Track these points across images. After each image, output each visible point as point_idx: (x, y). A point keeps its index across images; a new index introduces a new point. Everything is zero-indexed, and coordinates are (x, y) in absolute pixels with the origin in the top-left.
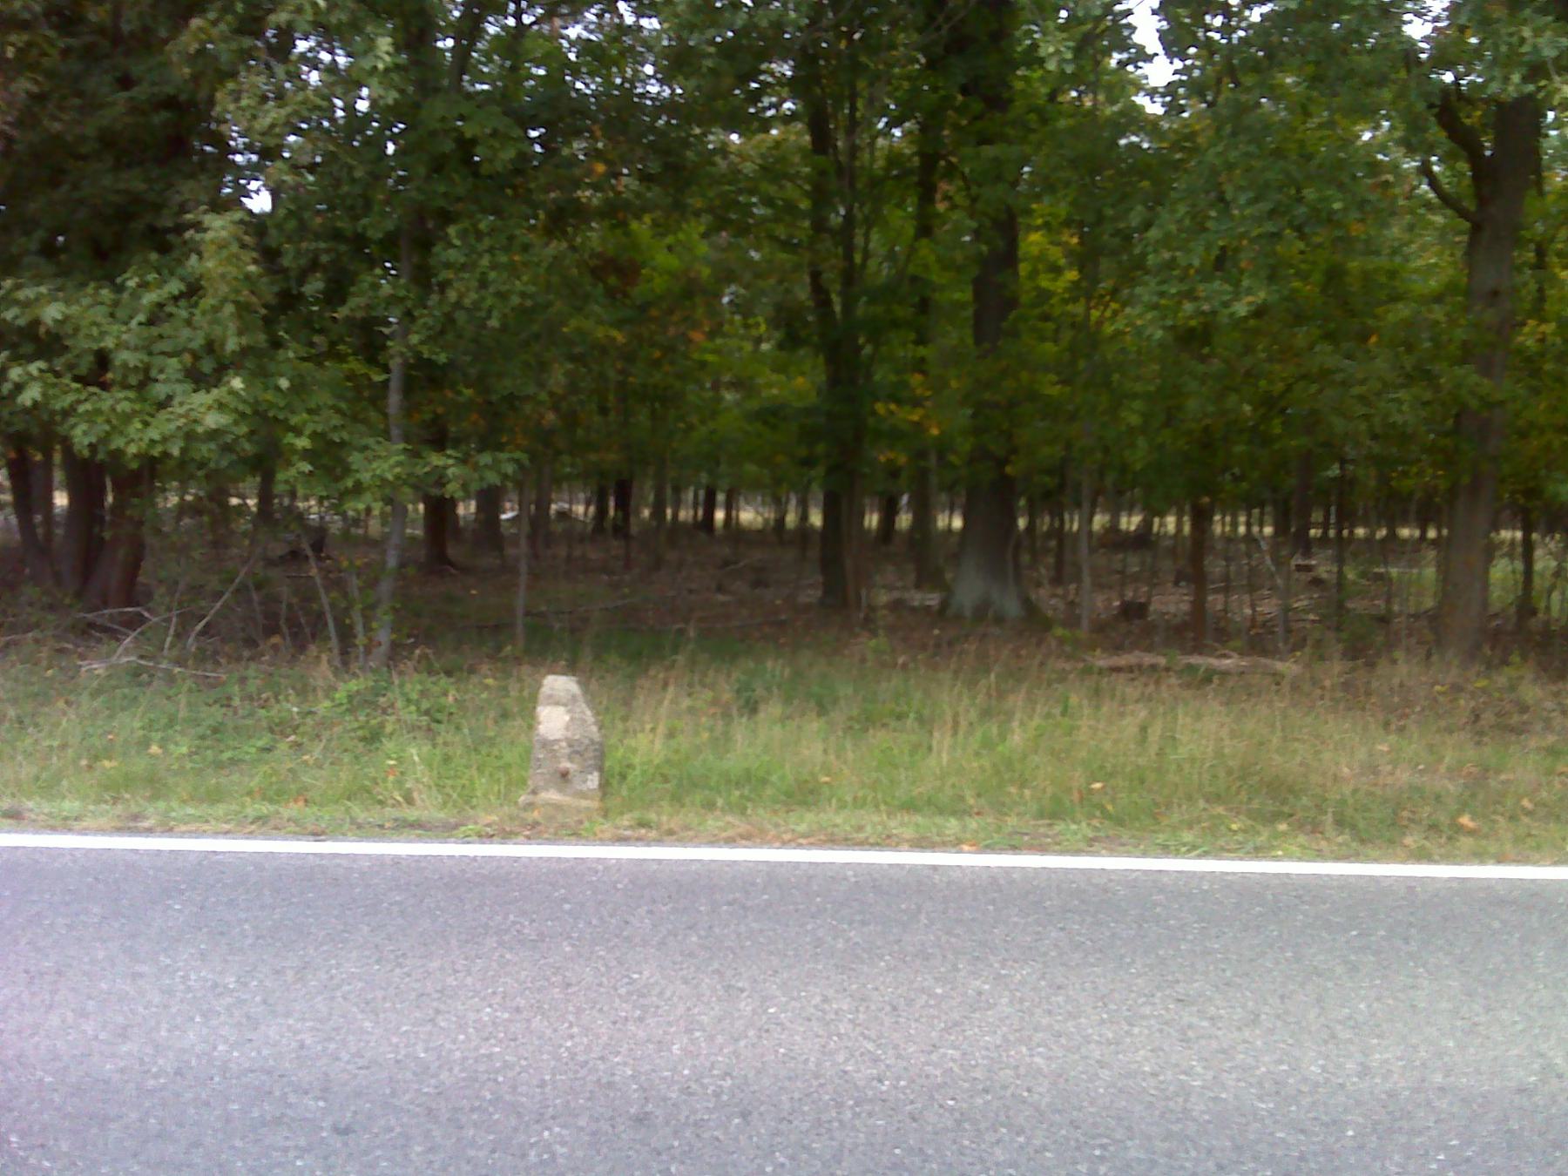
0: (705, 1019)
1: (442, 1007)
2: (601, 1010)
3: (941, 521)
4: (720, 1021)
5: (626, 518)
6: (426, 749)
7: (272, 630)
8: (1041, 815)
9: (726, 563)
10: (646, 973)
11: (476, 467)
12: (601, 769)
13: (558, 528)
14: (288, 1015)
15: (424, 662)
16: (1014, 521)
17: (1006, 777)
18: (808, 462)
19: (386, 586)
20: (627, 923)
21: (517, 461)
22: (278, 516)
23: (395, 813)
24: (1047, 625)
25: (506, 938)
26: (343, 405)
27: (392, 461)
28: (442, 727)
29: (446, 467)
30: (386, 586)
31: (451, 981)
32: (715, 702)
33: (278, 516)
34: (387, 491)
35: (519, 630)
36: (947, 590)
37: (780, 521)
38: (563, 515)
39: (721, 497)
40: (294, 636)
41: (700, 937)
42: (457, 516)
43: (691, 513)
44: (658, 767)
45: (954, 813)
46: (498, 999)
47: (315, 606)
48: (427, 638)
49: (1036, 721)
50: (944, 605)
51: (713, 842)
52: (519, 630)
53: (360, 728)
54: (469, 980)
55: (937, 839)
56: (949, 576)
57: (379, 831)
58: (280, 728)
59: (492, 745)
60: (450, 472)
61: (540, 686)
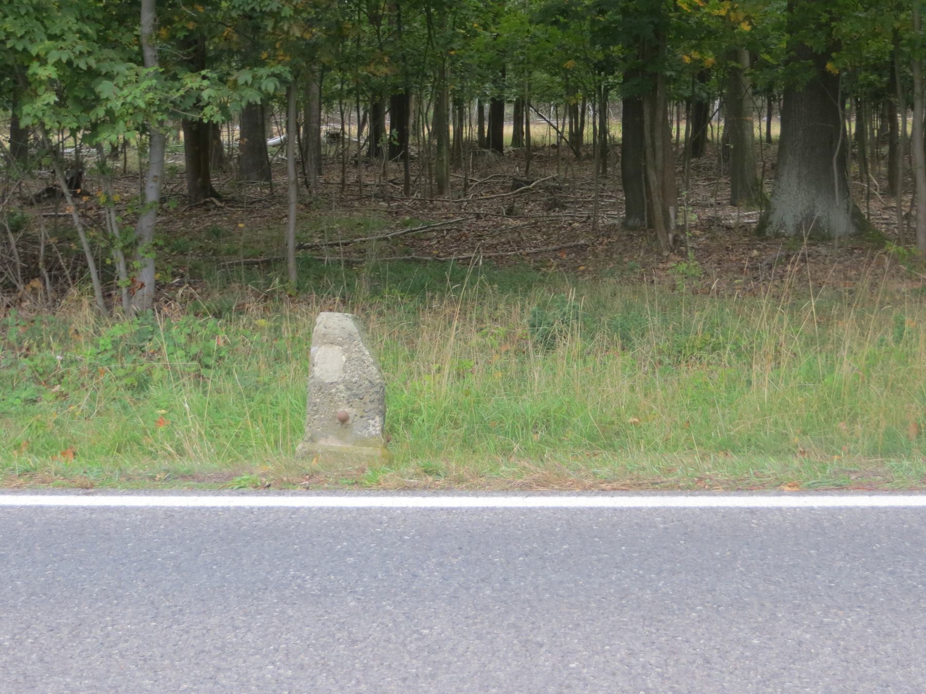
0: (501, 675)
1: (224, 665)
2: (390, 666)
3: (758, 129)
4: (517, 677)
5: (403, 137)
6: (196, 396)
7: (30, 274)
8: (874, 452)
9: (517, 184)
10: (437, 629)
11: (235, 86)
12: (383, 413)
13: (331, 151)
14: (64, 673)
15: (190, 304)
16: (838, 125)
17: (835, 412)
18: (606, 67)
19: (147, 222)
20: (415, 576)
21: (278, 76)
22: (32, 151)
23: (166, 464)
24: (880, 241)
25: (287, 593)
26: (89, 30)
27: (144, 85)
28: (211, 372)
29: (200, 89)
30: (147, 222)
31: (230, 637)
32: (508, 337)
33: (32, 151)
34: (140, 119)
35: (292, 264)
36: (765, 203)
37: (577, 135)
38: (335, 137)
39: (509, 110)
40: (54, 279)
41: (494, 590)
42: (219, 142)
43: (476, 128)
44: (446, 411)
45: (777, 453)
46: (280, 656)
47: (73, 246)
48: (195, 276)
49: (868, 349)
50: (763, 224)
51: (507, 489)
52: (292, 264)
53: (127, 375)
54: (250, 637)
55: (754, 480)
56: (767, 190)
57: (150, 485)
58: (42, 377)
59: (266, 391)
60: (205, 95)
61: (313, 323)
